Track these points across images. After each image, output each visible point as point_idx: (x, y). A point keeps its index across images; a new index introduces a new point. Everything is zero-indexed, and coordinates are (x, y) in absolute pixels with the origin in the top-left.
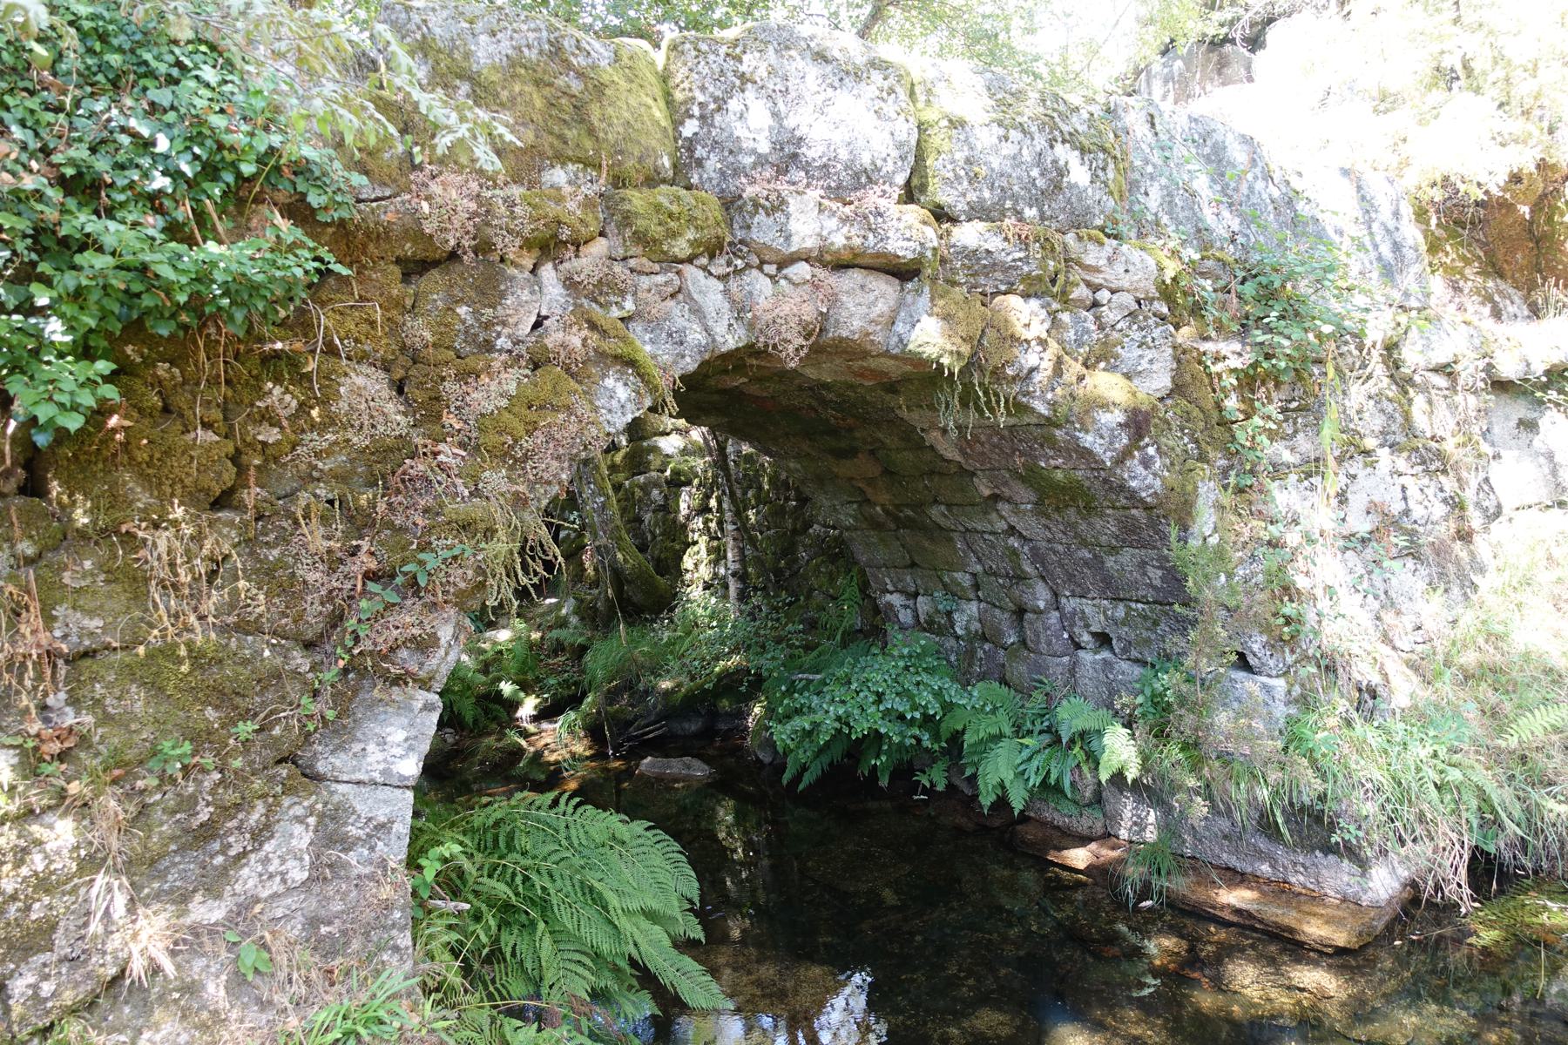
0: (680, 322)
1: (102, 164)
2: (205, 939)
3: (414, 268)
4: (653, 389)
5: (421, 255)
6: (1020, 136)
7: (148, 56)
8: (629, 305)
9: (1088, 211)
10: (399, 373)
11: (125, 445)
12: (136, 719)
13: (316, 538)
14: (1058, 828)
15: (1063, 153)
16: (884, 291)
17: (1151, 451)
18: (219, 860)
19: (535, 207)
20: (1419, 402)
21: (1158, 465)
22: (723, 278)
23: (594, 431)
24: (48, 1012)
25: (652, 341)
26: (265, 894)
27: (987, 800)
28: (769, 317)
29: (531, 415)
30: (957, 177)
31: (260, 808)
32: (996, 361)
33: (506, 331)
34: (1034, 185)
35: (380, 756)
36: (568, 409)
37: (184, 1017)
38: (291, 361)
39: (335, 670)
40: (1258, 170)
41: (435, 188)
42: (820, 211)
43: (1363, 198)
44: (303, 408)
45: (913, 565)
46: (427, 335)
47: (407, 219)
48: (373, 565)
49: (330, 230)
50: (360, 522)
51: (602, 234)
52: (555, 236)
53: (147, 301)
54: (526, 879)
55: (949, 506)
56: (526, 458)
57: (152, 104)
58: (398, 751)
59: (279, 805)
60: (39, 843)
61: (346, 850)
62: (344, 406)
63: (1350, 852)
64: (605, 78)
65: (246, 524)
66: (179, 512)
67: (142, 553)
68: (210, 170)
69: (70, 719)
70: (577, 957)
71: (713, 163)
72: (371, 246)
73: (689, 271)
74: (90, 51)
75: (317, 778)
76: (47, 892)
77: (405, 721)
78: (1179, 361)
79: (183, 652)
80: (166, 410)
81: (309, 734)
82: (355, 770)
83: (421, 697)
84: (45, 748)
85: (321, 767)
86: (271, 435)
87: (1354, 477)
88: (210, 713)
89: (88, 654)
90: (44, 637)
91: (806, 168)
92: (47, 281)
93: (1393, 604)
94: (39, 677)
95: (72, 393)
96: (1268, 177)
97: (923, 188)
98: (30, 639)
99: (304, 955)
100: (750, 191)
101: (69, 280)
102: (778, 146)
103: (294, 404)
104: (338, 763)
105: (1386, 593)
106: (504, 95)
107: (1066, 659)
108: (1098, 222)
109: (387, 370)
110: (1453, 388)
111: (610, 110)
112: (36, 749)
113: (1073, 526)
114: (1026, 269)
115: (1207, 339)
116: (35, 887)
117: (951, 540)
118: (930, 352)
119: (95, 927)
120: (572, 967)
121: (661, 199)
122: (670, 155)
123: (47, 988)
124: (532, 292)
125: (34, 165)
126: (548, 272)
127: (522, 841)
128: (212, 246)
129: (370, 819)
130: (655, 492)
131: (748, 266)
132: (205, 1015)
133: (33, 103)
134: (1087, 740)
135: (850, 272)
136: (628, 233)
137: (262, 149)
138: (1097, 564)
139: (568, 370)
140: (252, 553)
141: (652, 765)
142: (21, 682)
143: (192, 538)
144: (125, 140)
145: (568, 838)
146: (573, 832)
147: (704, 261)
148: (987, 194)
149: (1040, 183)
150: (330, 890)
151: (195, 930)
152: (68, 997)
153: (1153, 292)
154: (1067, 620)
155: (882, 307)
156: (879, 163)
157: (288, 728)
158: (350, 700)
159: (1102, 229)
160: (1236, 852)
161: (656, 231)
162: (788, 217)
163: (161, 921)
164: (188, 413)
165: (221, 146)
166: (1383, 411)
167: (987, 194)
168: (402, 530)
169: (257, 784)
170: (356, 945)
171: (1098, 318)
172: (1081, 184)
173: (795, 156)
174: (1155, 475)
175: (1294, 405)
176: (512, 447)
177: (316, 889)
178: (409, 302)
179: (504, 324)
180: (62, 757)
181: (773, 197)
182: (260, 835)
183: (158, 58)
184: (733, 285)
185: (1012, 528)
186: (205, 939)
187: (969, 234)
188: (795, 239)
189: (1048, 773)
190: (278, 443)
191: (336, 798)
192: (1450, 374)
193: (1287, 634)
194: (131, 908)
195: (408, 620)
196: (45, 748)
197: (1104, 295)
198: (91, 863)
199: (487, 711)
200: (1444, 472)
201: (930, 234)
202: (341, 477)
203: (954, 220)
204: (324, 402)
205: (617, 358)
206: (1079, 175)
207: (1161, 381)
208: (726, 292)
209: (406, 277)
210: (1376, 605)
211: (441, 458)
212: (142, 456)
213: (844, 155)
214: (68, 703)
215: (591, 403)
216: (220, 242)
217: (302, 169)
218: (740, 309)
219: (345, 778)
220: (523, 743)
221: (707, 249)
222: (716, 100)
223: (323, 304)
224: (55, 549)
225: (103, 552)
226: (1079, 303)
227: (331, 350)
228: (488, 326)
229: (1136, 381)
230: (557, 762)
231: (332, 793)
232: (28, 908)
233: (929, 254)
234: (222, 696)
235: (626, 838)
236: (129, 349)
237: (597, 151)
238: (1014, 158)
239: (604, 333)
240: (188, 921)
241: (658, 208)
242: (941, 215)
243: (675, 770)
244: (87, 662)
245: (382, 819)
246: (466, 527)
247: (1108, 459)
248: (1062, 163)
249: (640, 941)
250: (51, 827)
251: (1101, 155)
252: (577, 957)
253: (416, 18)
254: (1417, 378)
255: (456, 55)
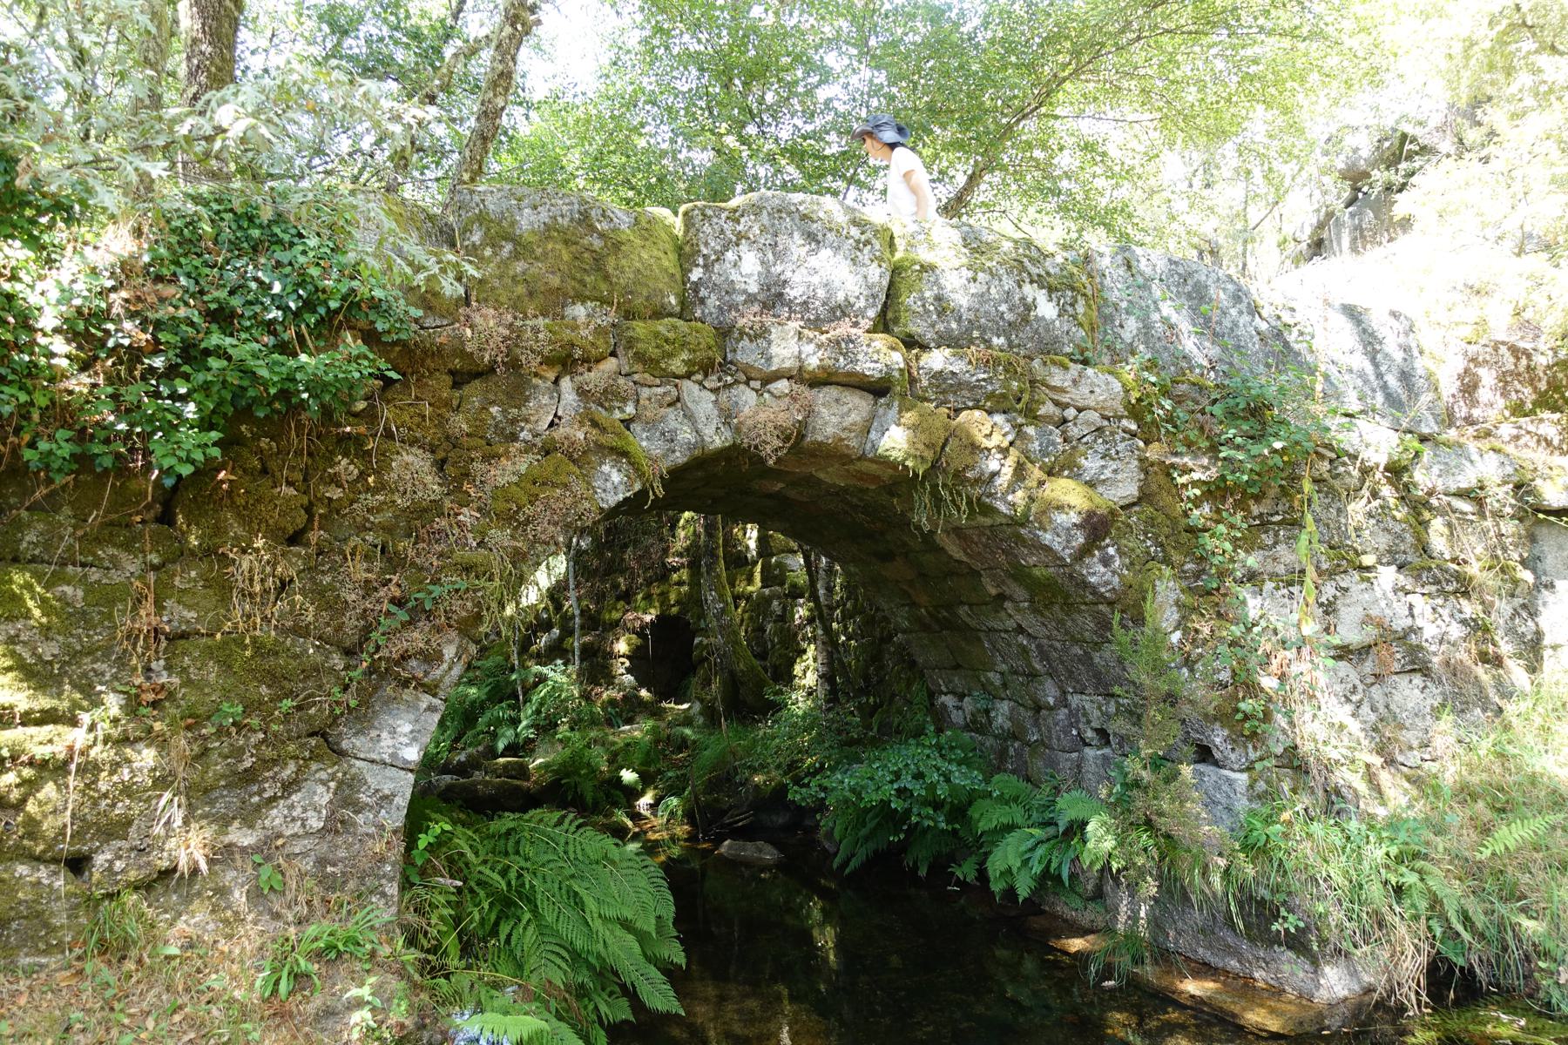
0: (673, 424)
1: (236, 302)
2: (237, 856)
3: (460, 379)
4: (641, 475)
5: (467, 368)
6: (988, 277)
7: (277, 230)
8: (630, 409)
9: (1056, 340)
10: (441, 454)
11: (230, 493)
12: (208, 685)
13: (359, 571)
14: (1066, 921)
15: (1029, 290)
16: (857, 406)
17: (1111, 551)
18: (256, 799)
19: (554, 333)
20: (1437, 524)
21: (1117, 563)
22: (715, 391)
23: (587, 505)
24: (117, 882)
25: (648, 438)
26: (288, 833)
27: (997, 887)
28: (750, 422)
29: (535, 489)
30: (927, 312)
31: (291, 767)
32: (957, 464)
33: (528, 426)
34: (1002, 318)
35: (390, 742)
36: (566, 486)
37: (213, 911)
38: (358, 440)
39: (360, 670)
40: (1243, 306)
41: (478, 319)
42: (800, 339)
43: (1364, 331)
44: (363, 475)
45: (957, 667)
46: (464, 426)
47: (456, 342)
48: (398, 594)
49: (397, 349)
50: (394, 562)
51: (613, 354)
52: (570, 355)
53: (251, 393)
54: (520, 876)
55: (971, 605)
56: (527, 522)
57: (278, 262)
58: (405, 740)
59: (307, 767)
60: (128, 761)
61: (357, 812)
62: (394, 476)
63: (1296, 943)
64: (624, 237)
65: (309, 556)
66: (259, 543)
67: (231, 569)
68: (308, 305)
69: (164, 679)
70: (557, 949)
71: (713, 301)
72: (428, 361)
73: (687, 385)
74: (240, 227)
75: (342, 754)
76: (129, 796)
77: (412, 717)
78: (1147, 473)
79: (247, 641)
80: (265, 471)
81: (336, 718)
82: (370, 750)
83: (426, 700)
84: (144, 696)
85: (345, 745)
86: (335, 493)
87: (1346, 590)
88: (264, 690)
89: (184, 636)
90: (154, 620)
91: (789, 304)
92: (187, 377)
93: (1395, 718)
94: (147, 648)
95: (189, 451)
96: (1254, 310)
97: (896, 321)
98: (145, 619)
99: (309, 883)
100: (741, 322)
101: (201, 377)
102: (766, 287)
103: (356, 472)
104: (358, 744)
105: (1387, 707)
106: (539, 251)
107: (1075, 755)
108: (1068, 350)
109: (433, 452)
110: (1481, 514)
111: (624, 262)
112: (137, 696)
113: (1061, 622)
114: (990, 388)
115: (1176, 454)
116: (121, 792)
117: (979, 639)
118: (897, 455)
119: (158, 830)
120: (553, 957)
121: (661, 329)
122: (677, 295)
123: (119, 865)
124: (552, 398)
125: (192, 302)
126: (566, 384)
127: (527, 849)
128: (303, 358)
129: (377, 791)
130: (775, 603)
131: (736, 382)
132: (229, 913)
133: (197, 262)
134: (1077, 829)
135: (826, 389)
136: (630, 354)
137: (344, 290)
138: (1086, 659)
139: (570, 458)
140: (312, 578)
141: (730, 847)
142: (134, 649)
143: (268, 562)
144: (253, 285)
145: (566, 852)
146: (571, 848)
147: (699, 377)
148: (954, 325)
149: (1009, 316)
150: (340, 840)
151: (229, 847)
152: (133, 875)
153: (1121, 410)
154: (1076, 715)
155: (854, 417)
156: (852, 300)
157: (321, 710)
158: (371, 696)
159: (1068, 355)
160: (1210, 947)
161: (653, 352)
162: (770, 343)
163: (208, 833)
164: (278, 474)
165: (317, 290)
166: (1386, 530)
167: (954, 325)
168: (421, 569)
169: (291, 747)
170: (351, 885)
171: (1064, 432)
172: (1047, 317)
173: (781, 295)
174: (1114, 572)
175: (1277, 518)
176: (517, 512)
177: (329, 838)
178: (455, 403)
179: (527, 421)
180: (155, 704)
181: (756, 327)
182: (289, 787)
183: (284, 231)
184: (723, 396)
185: (1020, 626)
186: (237, 856)
187: (937, 359)
188: (775, 360)
189: (1050, 861)
190: (340, 499)
191: (353, 771)
192: (1475, 499)
193: (1249, 731)
194: (186, 822)
195: (417, 638)
196: (144, 696)
197: (1070, 413)
198: (162, 783)
199: (608, 795)
200: (1466, 594)
201: (897, 359)
202: (388, 529)
203: (924, 347)
204: (377, 473)
205: (612, 450)
206: (1047, 309)
207: (1126, 488)
208: (716, 402)
209: (456, 385)
210: (1373, 717)
211: (461, 518)
212: (240, 501)
213: (821, 293)
214: (165, 668)
215: (589, 483)
216: (311, 355)
217: (375, 304)
218: (727, 416)
219: (362, 756)
220: (630, 823)
221: (701, 368)
222: (716, 252)
223: (388, 402)
224: (174, 562)
225: (204, 566)
226: (1048, 419)
227: (389, 435)
228: (514, 422)
229: (1100, 489)
230: (656, 841)
231: (351, 766)
232: (113, 805)
233: (896, 374)
234: (272, 678)
235: (617, 859)
236: (243, 428)
237: (611, 292)
238: (982, 295)
239: (604, 430)
240: (227, 840)
241: (657, 335)
242: (910, 342)
243: (748, 853)
244: (183, 642)
245: (387, 792)
246: (467, 569)
247: (1067, 555)
248: (1030, 300)
249: (609, 942)
250: (139, 753)
251: (1069, 293)
252: (557, 949)
253: (477, 198)
254: (1434, 502)
255: (504, 223)
